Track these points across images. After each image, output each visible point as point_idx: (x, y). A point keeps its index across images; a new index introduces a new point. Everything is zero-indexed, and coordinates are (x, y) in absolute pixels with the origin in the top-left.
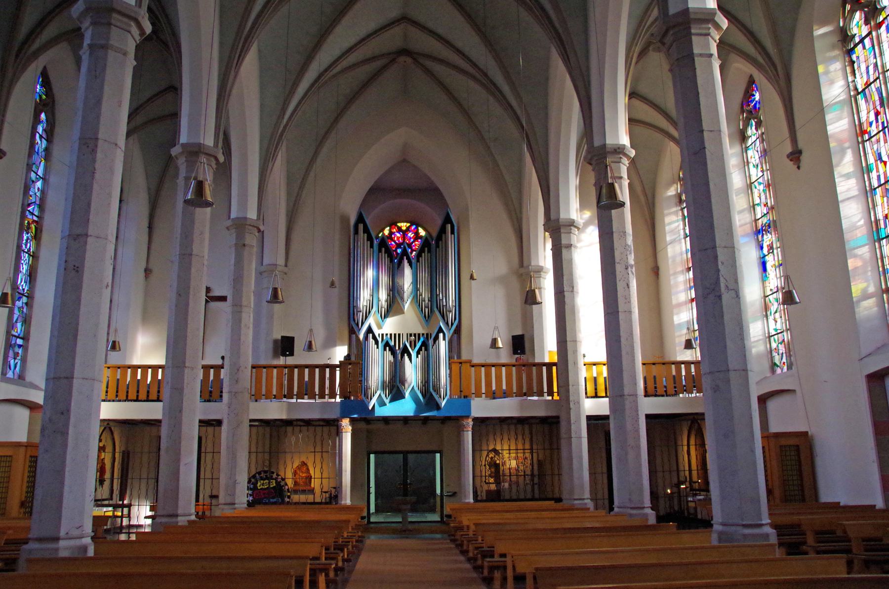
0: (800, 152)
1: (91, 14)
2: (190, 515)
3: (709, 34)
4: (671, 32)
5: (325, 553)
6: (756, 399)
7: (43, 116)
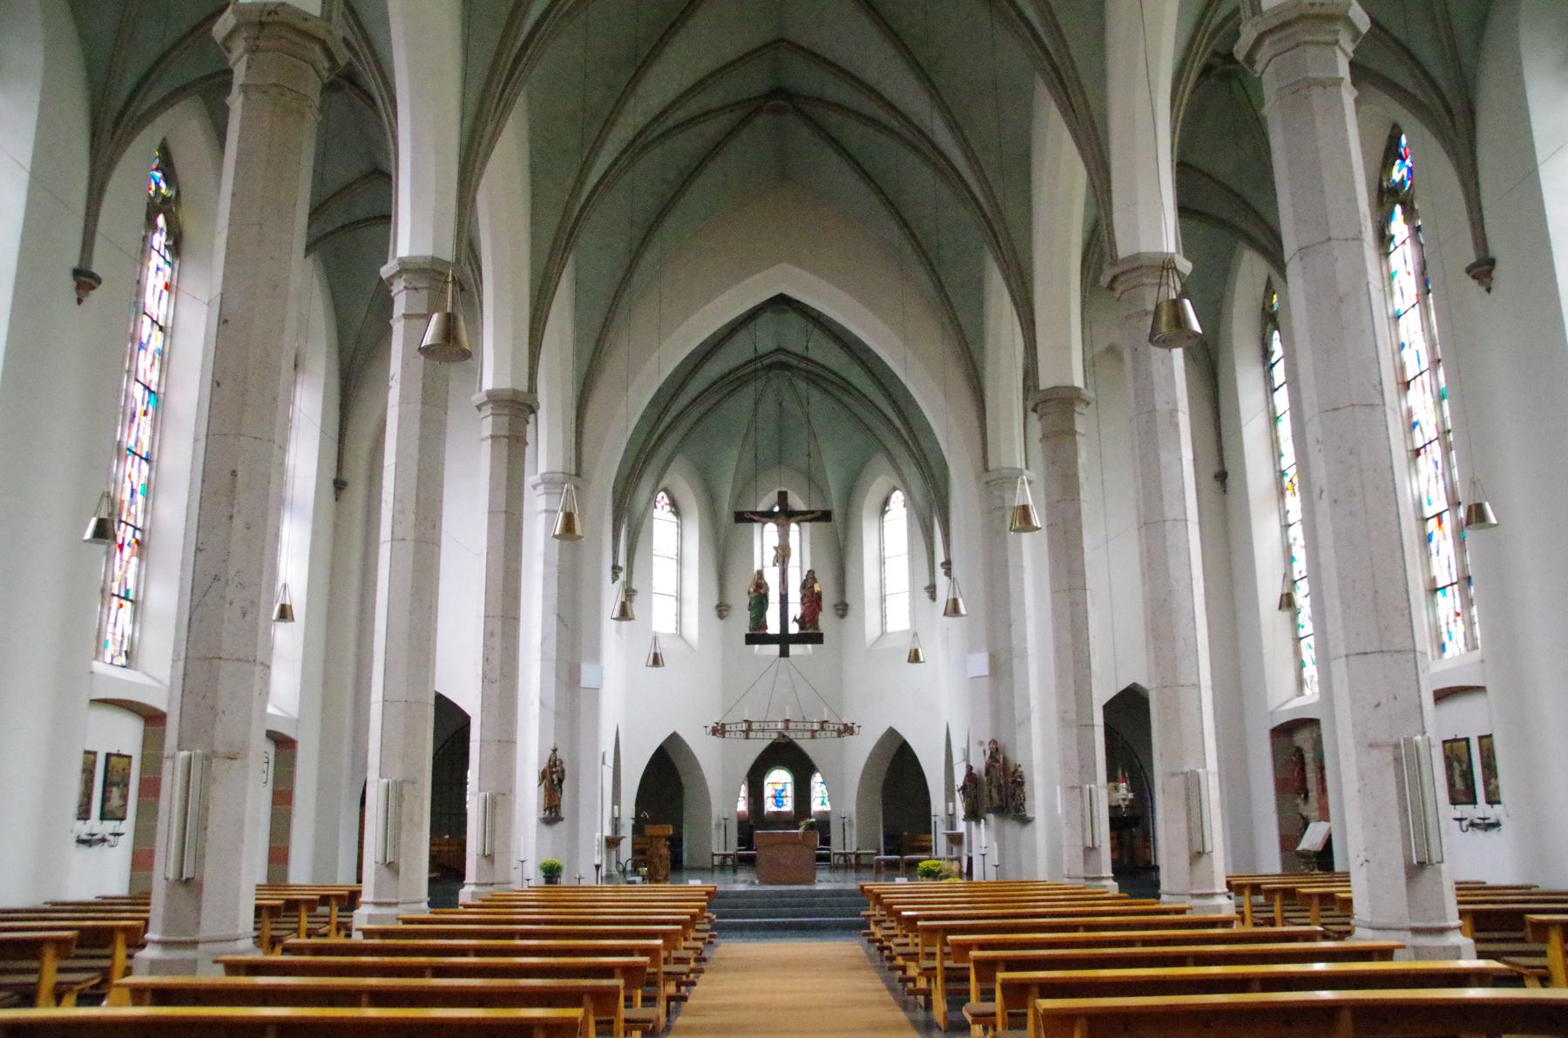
0: (1492, 262)
1: (245, 35)
2: (420, 902)
3: (1336, 42)
4: (1267, 42)
5: (597, 1023)
6: (984, 1004)
7: (161, 221)
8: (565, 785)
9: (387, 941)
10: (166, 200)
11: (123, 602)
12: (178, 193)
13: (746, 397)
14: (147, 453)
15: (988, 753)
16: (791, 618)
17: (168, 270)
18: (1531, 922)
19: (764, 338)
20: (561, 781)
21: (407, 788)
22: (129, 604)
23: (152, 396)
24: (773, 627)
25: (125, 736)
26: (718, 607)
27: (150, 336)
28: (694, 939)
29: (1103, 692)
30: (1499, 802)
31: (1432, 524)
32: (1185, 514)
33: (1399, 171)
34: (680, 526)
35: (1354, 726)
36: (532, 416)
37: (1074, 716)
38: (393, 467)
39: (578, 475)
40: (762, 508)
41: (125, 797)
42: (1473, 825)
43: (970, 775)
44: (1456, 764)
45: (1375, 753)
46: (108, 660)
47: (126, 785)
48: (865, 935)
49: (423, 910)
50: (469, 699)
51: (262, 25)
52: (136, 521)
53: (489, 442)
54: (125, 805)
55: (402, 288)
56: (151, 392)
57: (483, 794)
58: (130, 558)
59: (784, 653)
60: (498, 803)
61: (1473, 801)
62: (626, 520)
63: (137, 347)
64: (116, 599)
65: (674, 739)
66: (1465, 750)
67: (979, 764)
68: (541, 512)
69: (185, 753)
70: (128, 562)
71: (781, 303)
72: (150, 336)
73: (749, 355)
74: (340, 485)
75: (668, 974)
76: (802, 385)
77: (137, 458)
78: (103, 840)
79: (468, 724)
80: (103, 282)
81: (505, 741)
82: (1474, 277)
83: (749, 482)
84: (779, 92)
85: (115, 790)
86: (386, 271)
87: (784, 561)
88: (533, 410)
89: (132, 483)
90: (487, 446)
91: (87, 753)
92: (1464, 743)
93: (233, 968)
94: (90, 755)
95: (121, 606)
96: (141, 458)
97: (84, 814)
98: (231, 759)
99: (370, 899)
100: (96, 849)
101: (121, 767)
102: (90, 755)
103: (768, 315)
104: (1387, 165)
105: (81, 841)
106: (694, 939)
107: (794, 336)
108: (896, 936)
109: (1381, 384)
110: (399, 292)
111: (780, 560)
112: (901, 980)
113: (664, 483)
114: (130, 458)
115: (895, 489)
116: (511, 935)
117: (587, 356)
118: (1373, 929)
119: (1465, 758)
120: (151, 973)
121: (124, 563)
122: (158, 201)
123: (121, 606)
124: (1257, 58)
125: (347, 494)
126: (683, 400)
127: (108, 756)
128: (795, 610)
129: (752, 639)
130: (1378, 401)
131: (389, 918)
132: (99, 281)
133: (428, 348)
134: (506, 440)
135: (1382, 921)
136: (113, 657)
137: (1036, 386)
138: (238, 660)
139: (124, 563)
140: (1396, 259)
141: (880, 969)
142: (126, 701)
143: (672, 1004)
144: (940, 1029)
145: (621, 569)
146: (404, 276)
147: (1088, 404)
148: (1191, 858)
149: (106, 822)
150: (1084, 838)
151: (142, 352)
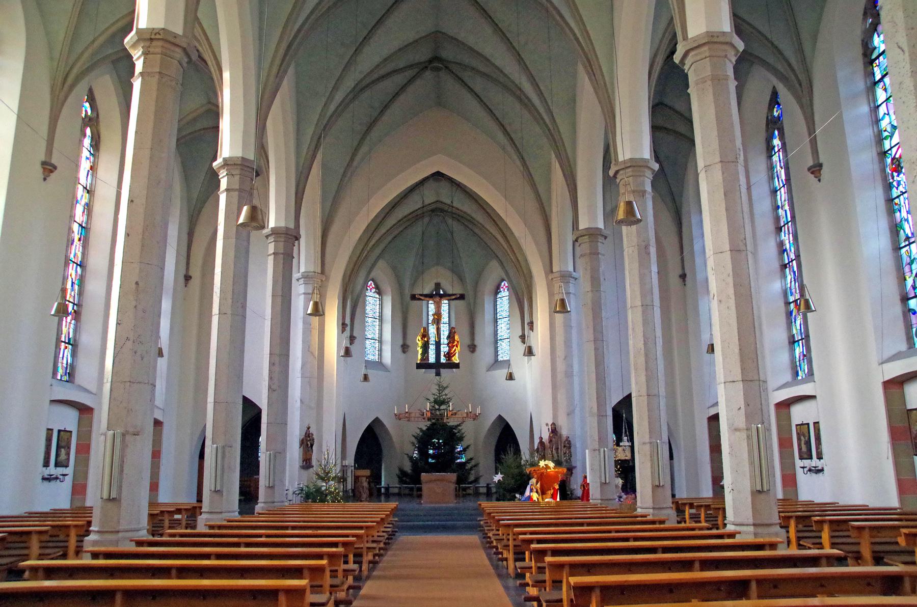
0: (821, 165)
3: (726, 56)
7: (88, 131)
8: (314, 448)
9: (219, 534)
10: (90, 119)
11: (67, 345)
12: (98, 115)
13: (418, 229)
14: (81, 262)
15: (550, 430)
16: (442, 354)
17: (92, 159)
18: (815, 521)
19: (429, 196)
20: (312, 445)
21: (227, 449)
22: (70, 346)
23: (83, 229)
24: (432, 359)
25: (69, 420)
26: (402, 346)
27: (82, 196)
28: (383, 532)
29: (615, 398)
30: (822, 458)
31: (792, 306)
32: (653, 301)
33: (777, 112)
34: (381, 300)
35: (728, 420)
36: (296, 242)
37: (596, 411)
38: (220, 274)
39: (323, 272)
40: (426, 292)
41: (68, 454)
42: (810, 470)
43: (541, 443)
44: (802, 438)
45: (738, 433)
46: (59, 378)
47: (69, 448)
48: (481, 531)
49: (236, 515)
50: (262, 401)
51: (151, 39)
52: (74, 300)
53: (272, 257)
54: (68, 459)
55: (225, 174)
56: (82, 227)
57: (269, 452)
58: (71, 321)
59: (438, 374)
60: (278, 455)
61: (811, 458)
62: (350, 297)
63: (75, 202)
64: (63, 344)
65: (377, 421)
66: (807, 430)
67: (546, 436)
68: (301, 294)
69: (111, 432)
70: (70, 323)
71: (438, 176)
72: (82, 196)
73: (419, 205)
74: (188, 278)
75: (368, 548)
76: (450, 221)
77: (75, 265)
78: (57, 478)
79: (261, 412)
80: (58, 168)
81: (281, 421)
82: (812, 173)
83: (419, 273)
84: (436, 59)
85: (63, 450)
86: (215, 164)
87: (438, 323)
88: (297, 238)
89: (72, 279)
90: (271, 260)
91: (48, 429)
92: (807, 426)
93: (140, 543)
94: (50, 430)
95: (66, 348)
96: (77, 264)
97: (46, 464)
98: (136, 435)
99: (207, 510)
100: (53, 483)
101: (66, 437)
102: (50, 430)
103: (431, 180)
104: (771, 109)
105: (44, 479)
106: (383, 532)
107: (445, 195)
108: (493, 530)
109: (745, 239)
110: (224, 177)
111: (436, 322)
112: (495, 553)
113: (373, 275)
114: (71, 265)
115: (503, 280)
116: (286, 528)
117: (329, 204)
118: (735, 525)
119: (807, 434)
120: (93, 546)
121: (68, 324)
122: (87, 120)
123: (66, 348)
124: (686, 62)
125: (191, 282)
126: (383, 230)
127: (59, 431)
128: (444, 349)
129: (419, 366)
130: (743, 248)
131: (218, 520)
132: (55, 168)
133: (242, 224)
134: (282, 256)
135: (739, 521)
136: (61, 376)
137: (577, 228)
138: (140, 383)
139: (68, 324)
140: (775, 158)
141: (485, 548)
142: (64, 400)
143: (371, 565)
144: (511, 577)
145: (347, 325)
146: (226, 168)
147: (606, 238)
148: (653, 488)
149: (57, 468)
150: (600, 477)
151: (78, 205)
